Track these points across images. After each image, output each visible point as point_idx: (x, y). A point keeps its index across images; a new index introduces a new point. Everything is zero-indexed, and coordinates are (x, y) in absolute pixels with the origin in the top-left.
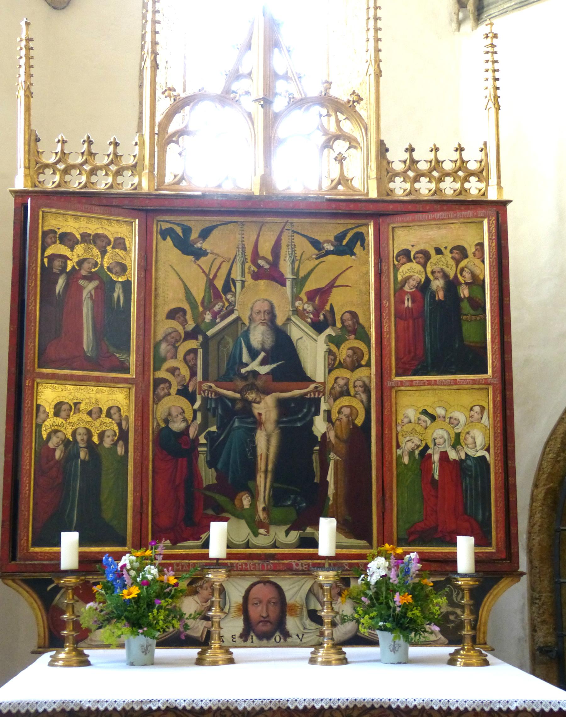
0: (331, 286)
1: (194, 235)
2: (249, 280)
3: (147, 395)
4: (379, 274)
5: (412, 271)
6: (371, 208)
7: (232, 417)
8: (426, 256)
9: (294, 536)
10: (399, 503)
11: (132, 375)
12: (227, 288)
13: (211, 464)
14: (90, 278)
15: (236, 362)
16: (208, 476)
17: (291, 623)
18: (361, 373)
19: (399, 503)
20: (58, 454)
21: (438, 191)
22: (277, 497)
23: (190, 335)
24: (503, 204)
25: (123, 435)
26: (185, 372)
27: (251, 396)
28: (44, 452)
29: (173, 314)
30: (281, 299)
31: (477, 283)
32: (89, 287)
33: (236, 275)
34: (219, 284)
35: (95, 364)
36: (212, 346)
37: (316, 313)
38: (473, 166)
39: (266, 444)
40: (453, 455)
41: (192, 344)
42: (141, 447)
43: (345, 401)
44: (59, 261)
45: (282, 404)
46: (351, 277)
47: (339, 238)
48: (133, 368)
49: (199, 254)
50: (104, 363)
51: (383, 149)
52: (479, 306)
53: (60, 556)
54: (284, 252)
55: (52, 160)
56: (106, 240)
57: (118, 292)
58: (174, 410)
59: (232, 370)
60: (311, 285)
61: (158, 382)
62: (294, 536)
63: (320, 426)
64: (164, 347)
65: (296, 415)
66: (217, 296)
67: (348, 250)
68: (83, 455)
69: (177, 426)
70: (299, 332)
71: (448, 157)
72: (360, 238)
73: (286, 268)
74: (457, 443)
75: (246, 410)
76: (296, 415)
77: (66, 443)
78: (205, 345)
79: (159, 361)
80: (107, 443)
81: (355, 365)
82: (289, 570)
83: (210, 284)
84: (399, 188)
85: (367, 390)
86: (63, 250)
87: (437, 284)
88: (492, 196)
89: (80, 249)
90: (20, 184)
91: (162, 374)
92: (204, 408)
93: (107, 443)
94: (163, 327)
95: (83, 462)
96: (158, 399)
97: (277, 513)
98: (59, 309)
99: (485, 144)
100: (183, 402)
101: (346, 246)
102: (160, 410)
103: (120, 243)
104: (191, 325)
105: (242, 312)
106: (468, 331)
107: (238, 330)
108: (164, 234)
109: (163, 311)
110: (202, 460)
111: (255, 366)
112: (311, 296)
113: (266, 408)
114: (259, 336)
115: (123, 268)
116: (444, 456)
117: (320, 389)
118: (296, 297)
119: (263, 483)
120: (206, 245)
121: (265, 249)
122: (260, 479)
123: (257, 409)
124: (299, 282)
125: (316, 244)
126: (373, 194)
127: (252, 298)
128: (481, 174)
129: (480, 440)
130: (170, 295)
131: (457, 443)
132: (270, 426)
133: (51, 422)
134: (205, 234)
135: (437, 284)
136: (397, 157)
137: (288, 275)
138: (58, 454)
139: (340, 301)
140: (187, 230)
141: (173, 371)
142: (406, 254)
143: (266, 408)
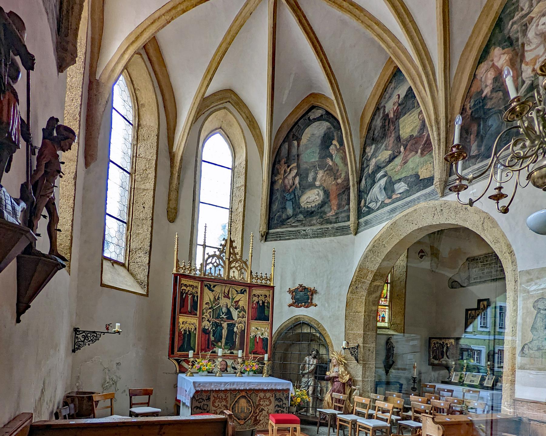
0: (239, 300)
1: (212, 287)
2: (223, 298)
3: (201, 320)
4: (249, 299)
5: (256, 299)
6: (249, 285)
7: (218, 326)
8: (259, 296)
9: (229, 351)
10: (248, 344)
11: (198, 316)
12: (218, 299)
13: (213, 336)
14: (190, 295)
15: (219, 315)
16: (212, 338)
17: (228, 369)
18: (244, 319)
19: (248, 344)
20: (183, 333)
21: (257, 282)
22: (226, 344)
23: (210, 308)
24: (273, 287)
25: (196, 329)
26: (209, 316)
27: (222, 322)
28: (180, 333)
29: (206, 304)
30: (229, 302)
31: (268, 303)
32: (190, 296)
33: (220, 296)
34: (217, 298)
35: (190, 313)
36: (215, 311)
37: (236, 306)
38: (268, 278)
39: (224, 332)
40: (261, 337)
41: (210, 310)
42: (199, 332)
43: (240, 324)
44: (337, 387)
45: (228, 324)
46: (242, 299)
47: (241, 290)
48: (387, 320)
49: (213, 291)
50: (193, 312)
51: (251, 272)
52: (268, 308)
53: (58, 70)
54: (230, 292)
55: (182, 266)
57: (196, 297)
58: (206, 324)
59: (218, 317)
60: (235, 300)
61: (203, 318)
62: (229, 351)
63: (235, 329)
64: (204, 311)
65: (231, 327)
66: (216, 300)
67: (243, 293)
68: (188, 333)
69: (207, 328)
70: (232, 309)
71: (264, 275)
72: (245, 290)
73: (230, 296)
74: (262, 334)
75: (221, 325)
76: (231, 327)
77: (184, 330)
78: (213, 311)
79: (203, 314)
80: (192, 331)
81: (243, 317)
82: (228, 358)
83: (215, 298)
84: (254, 281)
85: (245, 323)
86: (185, 288)
87: (261, 302)
88: (272, 285)
89: (188, 288)
90: (175, 272)
91: (204, 316)
92: (212, 324)
93: (192, 331)
94: (205, 306)
96: (203, 322)
97: (226, 347)
98: (183, 301)
100: (208, 322)
101: (242, 293)
102: (203, 324)
103: (197, 287)
104: (210, 306)
105: (221, 304)
106: (266, 312)
107: (220, 308)
108: (206, 286)
109: (204, 303)
110: (211, 335)
111: (223, 316)
112: (235, 302)
113: (225, 325)
114: (224, 310)
115: (197, 293)
116: (259, 337)
117: (236, 322)
118: (232, 302)
119: (223, 340)
120: (214, 289)
121: (226, 292)
122: (223, 339)
123: (223, 325)
124: (233, 299)
125: (237, 291)
126: (249, 282)
127: (223, 301)
128: (270, 280)
129: (267, 334)
130: (206, 299)
131: (262, 334)
132: (225, 329)
133: (181, 326)
134: (214, 287)
135: (261, 302)
136: (254, 274)
137: (231, 297)
138: (183, 333)
139: (241, 304)
140: (210, 285)
141: (206, 316)
142: (255, 295)
143: (225, 325)
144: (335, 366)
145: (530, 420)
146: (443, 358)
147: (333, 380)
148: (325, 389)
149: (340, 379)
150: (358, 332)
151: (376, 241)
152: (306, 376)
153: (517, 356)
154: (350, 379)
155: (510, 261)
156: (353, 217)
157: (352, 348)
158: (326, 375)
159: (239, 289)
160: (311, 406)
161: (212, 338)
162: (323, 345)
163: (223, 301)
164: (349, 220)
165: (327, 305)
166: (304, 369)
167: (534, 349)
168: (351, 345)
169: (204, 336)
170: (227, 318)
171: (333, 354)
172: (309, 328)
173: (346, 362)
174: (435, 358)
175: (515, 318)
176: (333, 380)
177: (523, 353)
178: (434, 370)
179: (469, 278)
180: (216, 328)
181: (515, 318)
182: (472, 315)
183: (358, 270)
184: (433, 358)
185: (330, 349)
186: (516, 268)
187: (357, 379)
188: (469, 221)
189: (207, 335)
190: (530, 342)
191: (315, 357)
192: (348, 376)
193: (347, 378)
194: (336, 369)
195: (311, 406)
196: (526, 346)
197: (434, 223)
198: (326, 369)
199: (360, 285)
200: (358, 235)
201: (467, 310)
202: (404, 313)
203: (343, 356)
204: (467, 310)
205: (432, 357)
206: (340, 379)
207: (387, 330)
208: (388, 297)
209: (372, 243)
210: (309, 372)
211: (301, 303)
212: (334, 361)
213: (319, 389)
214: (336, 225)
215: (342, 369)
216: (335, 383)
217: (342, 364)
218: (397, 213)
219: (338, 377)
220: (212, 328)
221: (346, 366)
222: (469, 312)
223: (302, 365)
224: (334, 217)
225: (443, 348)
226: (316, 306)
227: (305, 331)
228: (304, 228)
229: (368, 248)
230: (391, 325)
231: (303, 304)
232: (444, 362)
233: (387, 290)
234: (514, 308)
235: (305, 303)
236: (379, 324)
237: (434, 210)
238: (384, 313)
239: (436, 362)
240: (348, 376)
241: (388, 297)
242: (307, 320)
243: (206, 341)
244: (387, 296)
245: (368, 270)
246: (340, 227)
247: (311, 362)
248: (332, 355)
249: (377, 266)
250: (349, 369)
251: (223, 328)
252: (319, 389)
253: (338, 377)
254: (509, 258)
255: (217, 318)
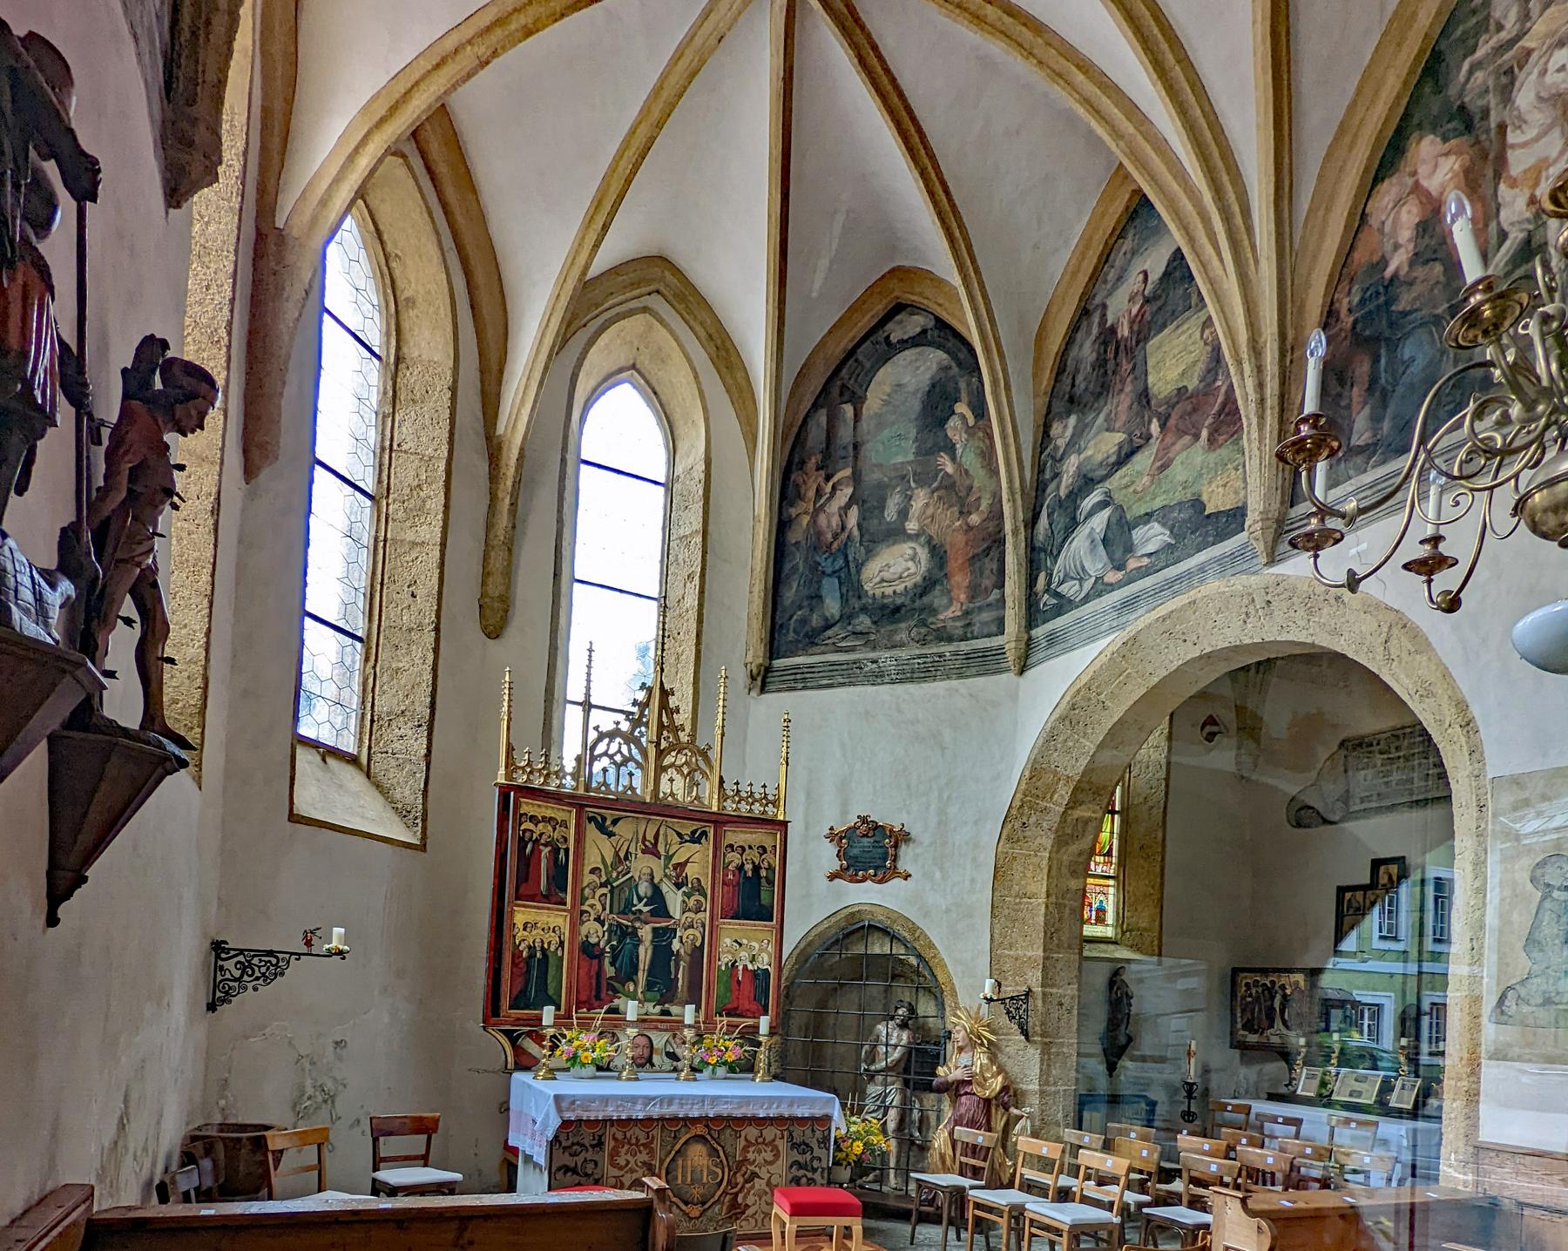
0: (687, 861)
1: (608, 823)
2: (640, 854)
3: (578, 917)
4: (715, 857)
5: (734, 858)
6: (714, 818)
7: (625, 935)
8: (743, 849)
9: (658, 1008)
10: (713, 988)
11: (569, 906)
12: (626, 858)
13: (612, 964)
14: (546, 845)
15: (629, 904)
16: (610, 971)
17: (656, 1059)
18: (701, 915)
19: (713, 988)
20: (525, 954)
21: (737, 809)
22: (649, 986)
23: (603, 885)
24: (785, 824)
25: (562, 944)
26: (599, 907)
27: (637, 925)
28: (517, 955)
29: (593, 871)
30: (657, 865)
31: (770, 868)
32: (546, 851)
33: (632, 850)
34: (622, 855)
35: (547, 898)
36: (616, 892)
37: (678, 877)
38: (770, 798)
39: (645, 954)
40: (750, 967)
41: (604, 890)
42: (571, 952)
43: (690, 931)
45: (655, 930)
46: (696, 858)
47: (693, 833)
48: (1110, 917)
49: (611, 835)
50: (553, 896)
51: (722, 781)
52: (771, 882)
54: (661, 838)
55: (523, 764)
57: (562, 853)
58: (593, 931)
59: (627, 909)
60: (674, 861)
61: (583, 912)
62: (658, 1008)
63: (676, 945)
64: (587, 891)
65: (663, 937)
66: (620, 862)
67: (698, 841)
68: (539, 955)
69: (593, 940)
70: (667, 888)
71: (758, 790)
72: (704, 833)
73: (661, 848)
74: (753, 960)
75: (634, 933)
76: (663, 937)
77: (530, 947)
78: (611, 892)
79: (584, 900)
80: (552, 948)
81: (698, 911)
82: (656, 1028)
83: (617, 854)
84: (730, 806)
85: (703, 926)
86: (531, 826)
87: (748, 867)
88: (781, 818)
89: (540, 826)
90: (501, 780)
91: (585, 908)
92: (610, 931)
93: (552, 948)
94: (588, 878)
95: (766, 1013)
96: (583, 923)
97: (649, 995)
98: (527, 864)
100: (597, 925)
101: (695, 840)
102: (584, 930)
103: (564, 824)
104: (604, 879)
105: (635, 873)
106: (764, 896)
107: (632, 884)
108: (590, 819)
109: (587, 869)
110: (607, 961)
111: (640, 906)
112: (676, 866)
113: (646, 932)
114: (644, 888)
115: (566, 840)
116: (745, 967)
117: (677, 923)
118: (666, 867)
119: (642, 977)
120: (615, 829)
121: (650, 837)
122: (640, 973)
123: (640, 933)
124: (669, 858)
125: (679, 835)
126: (715, 809)
127: (642, 865)
128: (775, 803)
129: (766, 959)
130: (592, 859)
131: (753, 960)
132: (647, 943)
133: (521, 934)
134: (615, 822)
135: (748, 867)
136: (729, 786)
137: (663, 852)
138: (525, 954)
139: (691, 871)
140: (604, 819)
141: (592, 906)
142: (731, 846)
143: (646, 932)
144: (961, 1049)
145: (1522, 1205)
146: (1271, 1026)
147: (955, 1089)
148: (933, 1117)
149: (975, 1088)
150: (1029, 954)
151: (1079, 691)
152: (879, 1078)
153: (1484, 1020)
154: (1005, 1089)
155: (1465, 748)
156: (1013, 623)
157: (1012, 998)
158: (935, 1075)
159: (687, 828)
160: (892, 1164)
161: (610, 971)
162: (929, 990)
163: (642, 865)
164: (1001, 631)
165: (938, 875)
166: (872, 1058)
167: (1532, 1002)
168: (1009, 990)
169: (585, 964)
170: (653, 913)
171: (956, 1015)
172: (887, 940)
173: (993, 1038)
174: (1249, 1026)
175: (1478, 913)
176: (957, 1089)
177: (1502, 1012)
178: (1245, 1061)
179: (1346, 798)
180: (619, 942)
181: (1478, 913)
182: (1355, 905)
183: (1027, 774)
184: (1244, 1027)
185: (948, 1001)
186: (1483, 769)
187: (1024, 1087)
188: (1346, 635)
189: (595, 962)
190: (1523, 982)
191: (903, 1026)
192: (1000, 1078)
193: (997, 1083)
194: (965, 1058)
195: (892, 1164)
196: (1510, 994)
197: (1247, 641)
198: (937, 1059)
199: (1033, 819)
200: (1029, 674)
201: (1341, 891)
202: (1161, 899)
203: (986, 1021)
204: (1341, 891)
205: (1239, 1026)
206: (975, 1088)
207: (1112, 947)
208: (1115, 853)
209: (1068, 698)
210: (887, 1069)
211: (866, 870)
212: (959, 1036)
213: (916, 1115)
214: (964, 647)
215: (981, 1059)
216: (963, 1099)
217: (982, 1044)
218: (1140, 612)
219: (970, 1083)
220: (609, 941)
221: (993, 1050)
222: (1348, 895)
223: (866, 1048)
224: (959, 624)
225: (1273, 998)
226: (907, 877)
227: (877, 950)
228: (872, 655)
229: (1058, 711)
230: (1123, 933)
231: (871, 872)
232: (1275, 1040)
233: (1112, 833)
234: (1477, 884)
235: (876, 868)
236: (1088, 930)
237: (1246, 601)
238: (1102, 898)
239: (1253, 1038)
240: (1000, 1078)
241: (1115, 853)
242: (880, 919)
243: (590, 978)
244: (1111, 849)
245: (1055, 773)
246: (975, 651)
247: (893, 1040)
248: (955, 1020)
249: (1084, 762)
250: (1002, 1058)
251: (640, 941)
252: (916, 1115)
253: (970, 1083)
254: (1463, 739)
255: (622, 913)
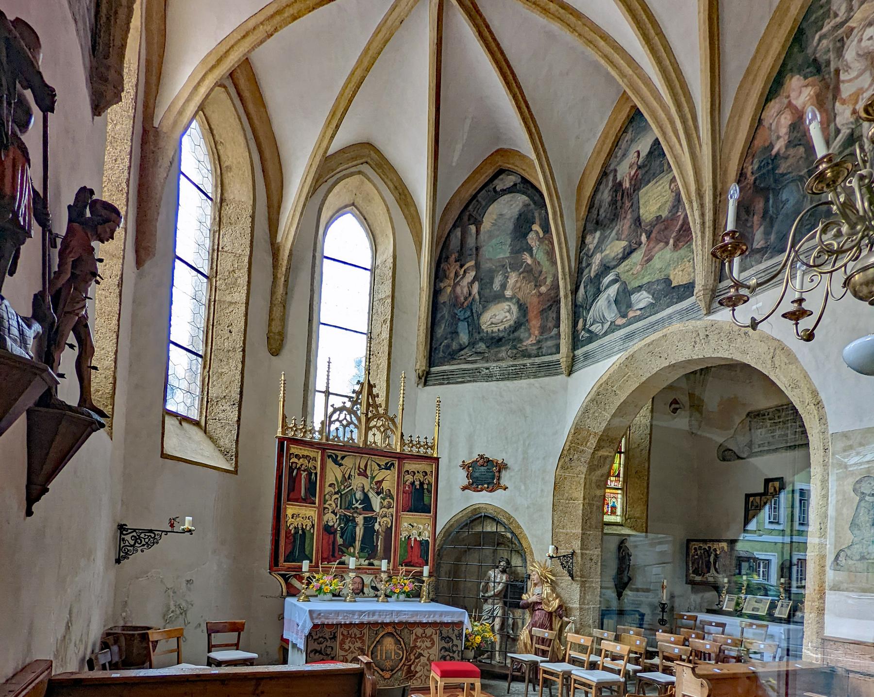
0: (383, 480)
1: (339, 458)
2: (357, 476)
3: (322, 511)
4: (398, 477)
5: (409, 478)
6: (398, 456)
7: (348, 521)
8: (414, 473)
9: (367, 562)
10: (397, 551)
11: (317, 505)
12: (349, 478)
13: (341, 537)
14: (304, 471)
15: (351, 503)
16: (340, 541)
17: (366, 590)
18: (391, 510)
19: (397, 551)
20: (292, 532)
21: (411, 451)
22: (362, 549)
23: (336, 493)
24: (437, 459)
25: (313, 526)
26: (334, 505)
27: (355, 515)
28: (288, 532)
29: (330, 485)
30: (366, 482)
31: (429, 484)
32: (304, 474)
33: (352, 473)
34: (347, 476)
35: (305, 500)
36: (343, 497)
37: (378, 488)
38: (429, 444)
39: (359, 531)
40: (418, 539)
41: (337, 496)
42: (318, 530)
43: (385, 519)
45: (365, 518)
46: (388, 478)
47: (387, 464)
48: (619, 511)
49: (341, 465)
50: (308, 499)
51: (402, 435)
52: (430, 492)
54: (368, 467)
55: (291, 426)
56: (24, 118)
57: (313, 475)
58: (330, 519)
59: (349, 506)
60: (376, 480)
61: (325, 508)
62: (367, 562)
63: (377, 527)
64: (327, 496)
65: (369, 522)
66: (346, 480)
67: (389, 469)
68: (300, 532)
69: (331, 524)
70: (372, 495)
71: (422, 440)
72: (393, 464)
73: (368, 473)
74: (420, 535)
75: (354, 520)
76: (369, 522)
77: (295, 528)
78: (341, 497)
79: (325, 501)
80: (308, 528)
81: (389, 507)
82: (366, 573)
83: (344, 476)
84: (407, 449)
85: (392, 516)
86: (296, 460)
87: (417, 483)
88: (435, 456)
89: (301, 460)
90: (279, 435)
91: (326, 506)
92: (340, 519)
93: (308, 528)
94: (328, 489)
96: (325, 514)
97: (362, 554)
98: (294, 481)
99: (29, 513)
100: (333, 515)
101: (387, 468)
102: (325, 518)
103: (315, 459)
104: (337, 490)
105: (354, 487)
106: (426, 499)
107: (352, 492)
108: (329, 457)
109: (327, 484)
110: (338, 535)
111: (357, 505)
112: (377, 483)
113: (360, 520)
114: (359, 495)
115: (315, 468)
116: (415, 539)
117: (377, 514)
118: (371, 483)
119: (358, 544)
120: (343, 462)
121: (362, 466)
122: (357, 542)
123: (357, 520)
124: (373, 478)
125: (379, 465)
126: (398, 451)
127: (358, 482)
128: (432, 448)
129: (427, 534)
130: (330, 479)
131: (420, 535)
132: (361, 525)
133: (290, 521)
134: (343, 458)
135: (417, 483)
136: (406, 438)
137: (369, 475)
138: (292, 532)
139: (385, 485)
140: (337, 456)
141: (330, 505)
142: (408, 471)
143: (360, 520)
144: (535, 585)
145: (848, 671)
146: (709, 572)
147: (532, 607)
148: (520, 622)
149: (543, 606)
150: (574, 531)
151: (601, 385)
152: (490, 601)
153: (827, 568)
154: (560, 607)
155: (817, 417)
156: (564, 347)
157: (564, 556)
158: (521, 599)
159: (383, 461)
160: (497, 649)
161: (340, 541)
162: (518, 552)
163: (358, 482)
164: (558, 352)
165: (523, 488)
166: (486, 590)
167: (854, 558)
168: (563, 552)
169: (326, 537)
170: (364, 509)
171: (533, 566)
172: (495, 524)
173: (553, 578)
174: (696, 572)
175: (824, 509)
176: (533, 607)
177: (837, 564)
178: (694, 591)
179: (750, 445)
180: (345, 525)
181: (824, 509)
182: (755, 504)
183: (572, 431)
184: (694, 572)
185: (528, 558)
186: (827, 428)
187: (571, 606)
188: (750, 354)
189: (332, 536)
190: (849, 547)
191: (504, 572)
192: (557, 601)
193: (556, 604)
194: (538, 590)
195: (497, 649)
196: (842, 554)
197: (695, 357)
198: (522, 590)
199: (576, 456)
200: (574, 375)
201: (748, 496)
202: (647, 501)
203: (549, 569)
204: (748, 496)
205: (691, 571)
206: (543, 606)
207: (620, 528)
208: (621, 475)
209: (595, 389)
210: (495, 595)
211: (482, 485)
212: (535, 577)
213: (510, 621)
214: (538, 360)
215: (547, 590)
216: (537, 612)
217: (547, 582)
218: (636, 341)
219: (540, 603)
220: (339, 524)
221: (553, 585)
222: (751, 499)
223: (483, 584)
224: (534, 348)
225: (709, 556)
226: (506, 488)
227: (489, 529)
228: (486, 365)
229: (590, 396)
230: (626, 520)
231: (486, 486)
232: (711, 579)
233: (620, 464)
234: (823, 492)
235: (488, 484)
236: (607, 518)
237: (694, 335)
238: (614, 500)
239: (698, 578)
240: (557, 601)
241: (621, 475)
242: (491, 512)
243: (329, 545)
244: (619, 473)
245: (588, 431)
246: (544, 363)
247: (498, 579)
248: (532, 568)
249: (604, 425)
250: (558, 590)
251: (357, 524)
252: (510, 621)
253: (540, 603)
254: (816, 412)
255: (347, 509)
